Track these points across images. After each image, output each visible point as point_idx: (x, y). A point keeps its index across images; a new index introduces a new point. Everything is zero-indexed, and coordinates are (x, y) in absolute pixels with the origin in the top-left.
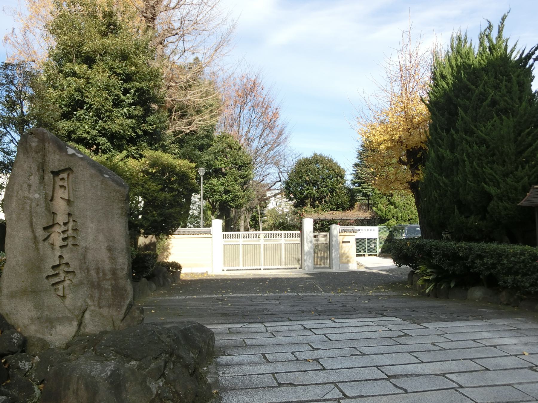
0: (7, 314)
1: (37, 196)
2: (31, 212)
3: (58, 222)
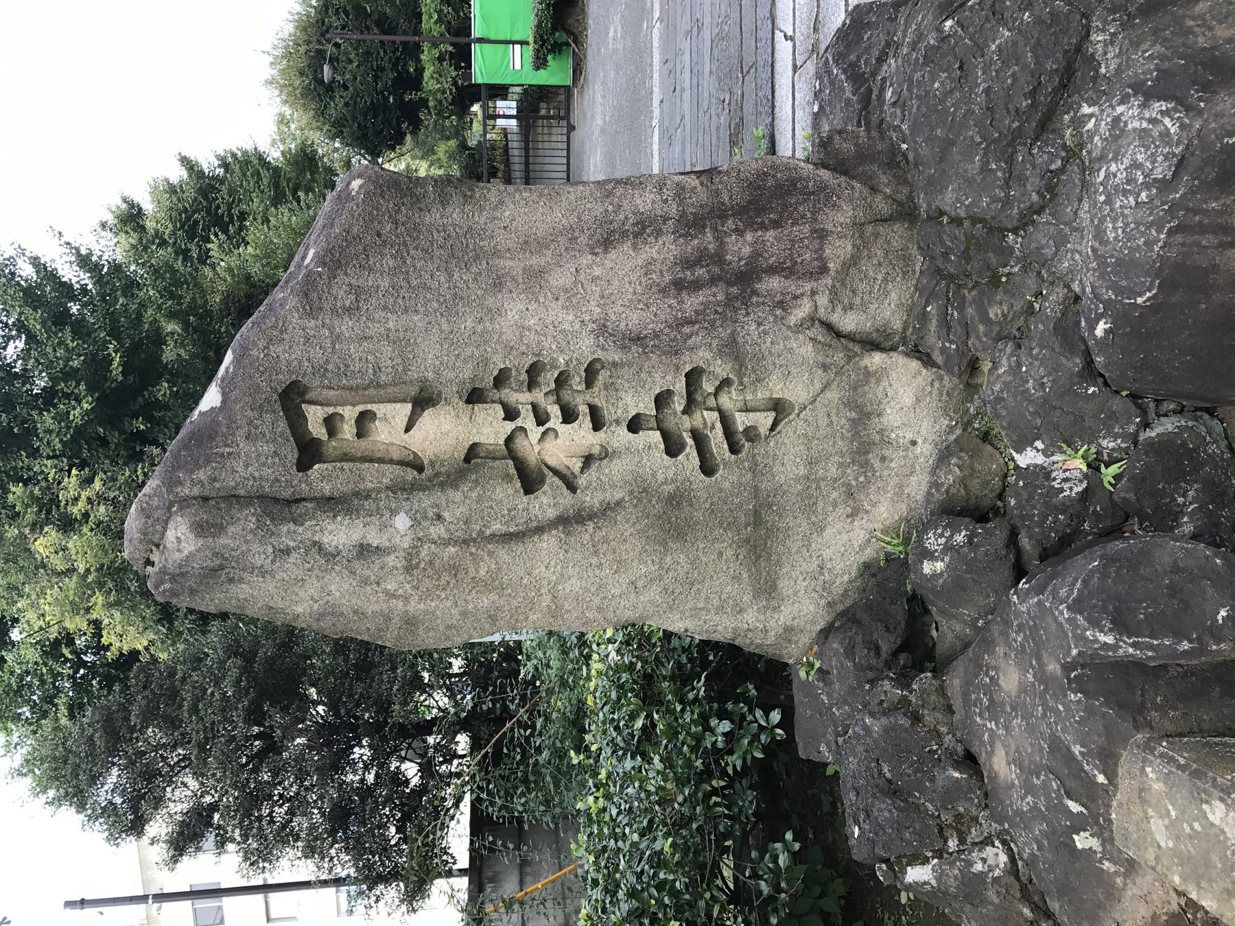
0: (829, 604)
1: (402, 522)
2: (465, 542)
3: (502, 442)
